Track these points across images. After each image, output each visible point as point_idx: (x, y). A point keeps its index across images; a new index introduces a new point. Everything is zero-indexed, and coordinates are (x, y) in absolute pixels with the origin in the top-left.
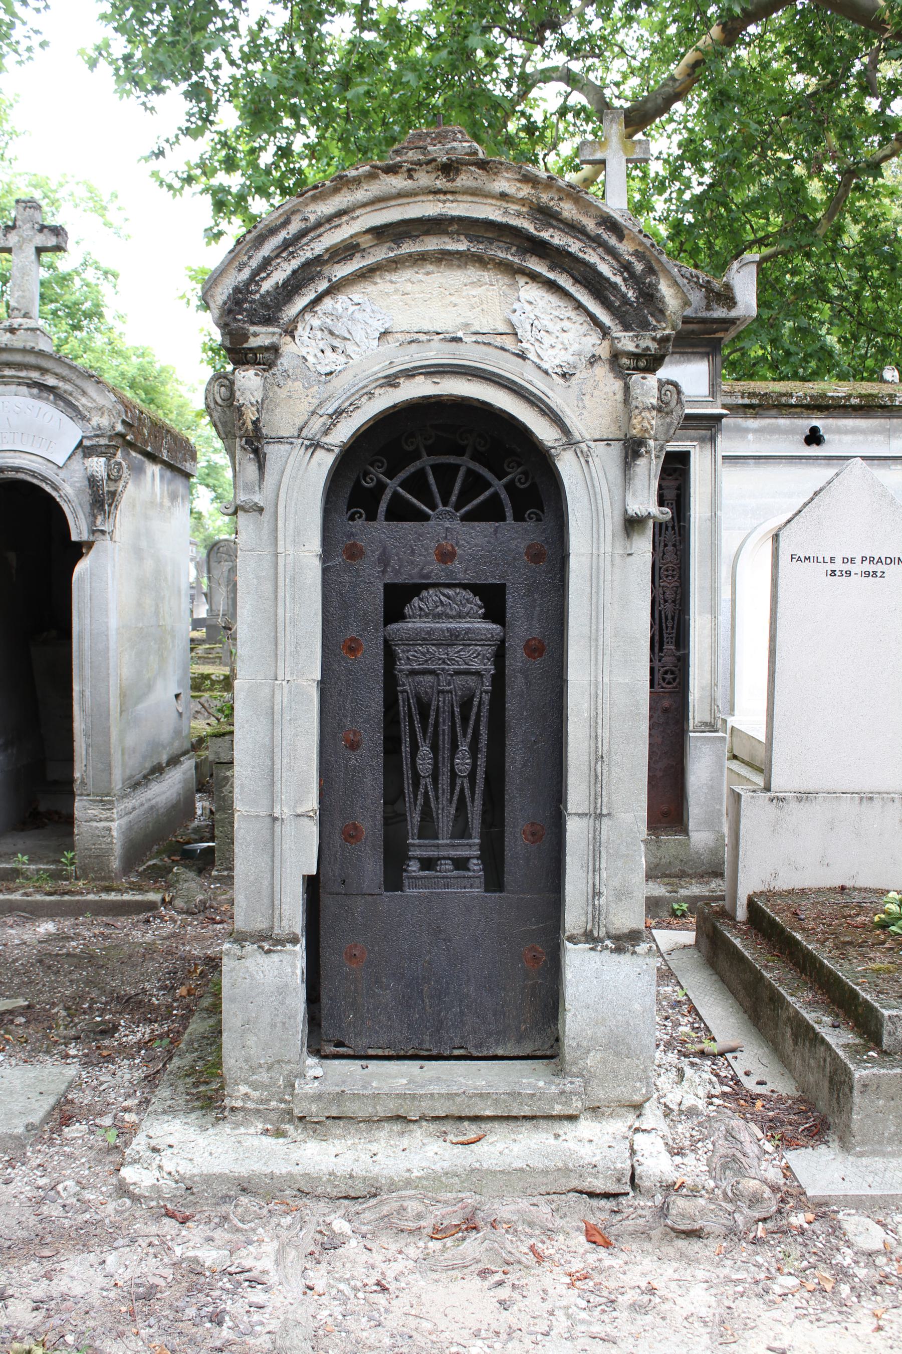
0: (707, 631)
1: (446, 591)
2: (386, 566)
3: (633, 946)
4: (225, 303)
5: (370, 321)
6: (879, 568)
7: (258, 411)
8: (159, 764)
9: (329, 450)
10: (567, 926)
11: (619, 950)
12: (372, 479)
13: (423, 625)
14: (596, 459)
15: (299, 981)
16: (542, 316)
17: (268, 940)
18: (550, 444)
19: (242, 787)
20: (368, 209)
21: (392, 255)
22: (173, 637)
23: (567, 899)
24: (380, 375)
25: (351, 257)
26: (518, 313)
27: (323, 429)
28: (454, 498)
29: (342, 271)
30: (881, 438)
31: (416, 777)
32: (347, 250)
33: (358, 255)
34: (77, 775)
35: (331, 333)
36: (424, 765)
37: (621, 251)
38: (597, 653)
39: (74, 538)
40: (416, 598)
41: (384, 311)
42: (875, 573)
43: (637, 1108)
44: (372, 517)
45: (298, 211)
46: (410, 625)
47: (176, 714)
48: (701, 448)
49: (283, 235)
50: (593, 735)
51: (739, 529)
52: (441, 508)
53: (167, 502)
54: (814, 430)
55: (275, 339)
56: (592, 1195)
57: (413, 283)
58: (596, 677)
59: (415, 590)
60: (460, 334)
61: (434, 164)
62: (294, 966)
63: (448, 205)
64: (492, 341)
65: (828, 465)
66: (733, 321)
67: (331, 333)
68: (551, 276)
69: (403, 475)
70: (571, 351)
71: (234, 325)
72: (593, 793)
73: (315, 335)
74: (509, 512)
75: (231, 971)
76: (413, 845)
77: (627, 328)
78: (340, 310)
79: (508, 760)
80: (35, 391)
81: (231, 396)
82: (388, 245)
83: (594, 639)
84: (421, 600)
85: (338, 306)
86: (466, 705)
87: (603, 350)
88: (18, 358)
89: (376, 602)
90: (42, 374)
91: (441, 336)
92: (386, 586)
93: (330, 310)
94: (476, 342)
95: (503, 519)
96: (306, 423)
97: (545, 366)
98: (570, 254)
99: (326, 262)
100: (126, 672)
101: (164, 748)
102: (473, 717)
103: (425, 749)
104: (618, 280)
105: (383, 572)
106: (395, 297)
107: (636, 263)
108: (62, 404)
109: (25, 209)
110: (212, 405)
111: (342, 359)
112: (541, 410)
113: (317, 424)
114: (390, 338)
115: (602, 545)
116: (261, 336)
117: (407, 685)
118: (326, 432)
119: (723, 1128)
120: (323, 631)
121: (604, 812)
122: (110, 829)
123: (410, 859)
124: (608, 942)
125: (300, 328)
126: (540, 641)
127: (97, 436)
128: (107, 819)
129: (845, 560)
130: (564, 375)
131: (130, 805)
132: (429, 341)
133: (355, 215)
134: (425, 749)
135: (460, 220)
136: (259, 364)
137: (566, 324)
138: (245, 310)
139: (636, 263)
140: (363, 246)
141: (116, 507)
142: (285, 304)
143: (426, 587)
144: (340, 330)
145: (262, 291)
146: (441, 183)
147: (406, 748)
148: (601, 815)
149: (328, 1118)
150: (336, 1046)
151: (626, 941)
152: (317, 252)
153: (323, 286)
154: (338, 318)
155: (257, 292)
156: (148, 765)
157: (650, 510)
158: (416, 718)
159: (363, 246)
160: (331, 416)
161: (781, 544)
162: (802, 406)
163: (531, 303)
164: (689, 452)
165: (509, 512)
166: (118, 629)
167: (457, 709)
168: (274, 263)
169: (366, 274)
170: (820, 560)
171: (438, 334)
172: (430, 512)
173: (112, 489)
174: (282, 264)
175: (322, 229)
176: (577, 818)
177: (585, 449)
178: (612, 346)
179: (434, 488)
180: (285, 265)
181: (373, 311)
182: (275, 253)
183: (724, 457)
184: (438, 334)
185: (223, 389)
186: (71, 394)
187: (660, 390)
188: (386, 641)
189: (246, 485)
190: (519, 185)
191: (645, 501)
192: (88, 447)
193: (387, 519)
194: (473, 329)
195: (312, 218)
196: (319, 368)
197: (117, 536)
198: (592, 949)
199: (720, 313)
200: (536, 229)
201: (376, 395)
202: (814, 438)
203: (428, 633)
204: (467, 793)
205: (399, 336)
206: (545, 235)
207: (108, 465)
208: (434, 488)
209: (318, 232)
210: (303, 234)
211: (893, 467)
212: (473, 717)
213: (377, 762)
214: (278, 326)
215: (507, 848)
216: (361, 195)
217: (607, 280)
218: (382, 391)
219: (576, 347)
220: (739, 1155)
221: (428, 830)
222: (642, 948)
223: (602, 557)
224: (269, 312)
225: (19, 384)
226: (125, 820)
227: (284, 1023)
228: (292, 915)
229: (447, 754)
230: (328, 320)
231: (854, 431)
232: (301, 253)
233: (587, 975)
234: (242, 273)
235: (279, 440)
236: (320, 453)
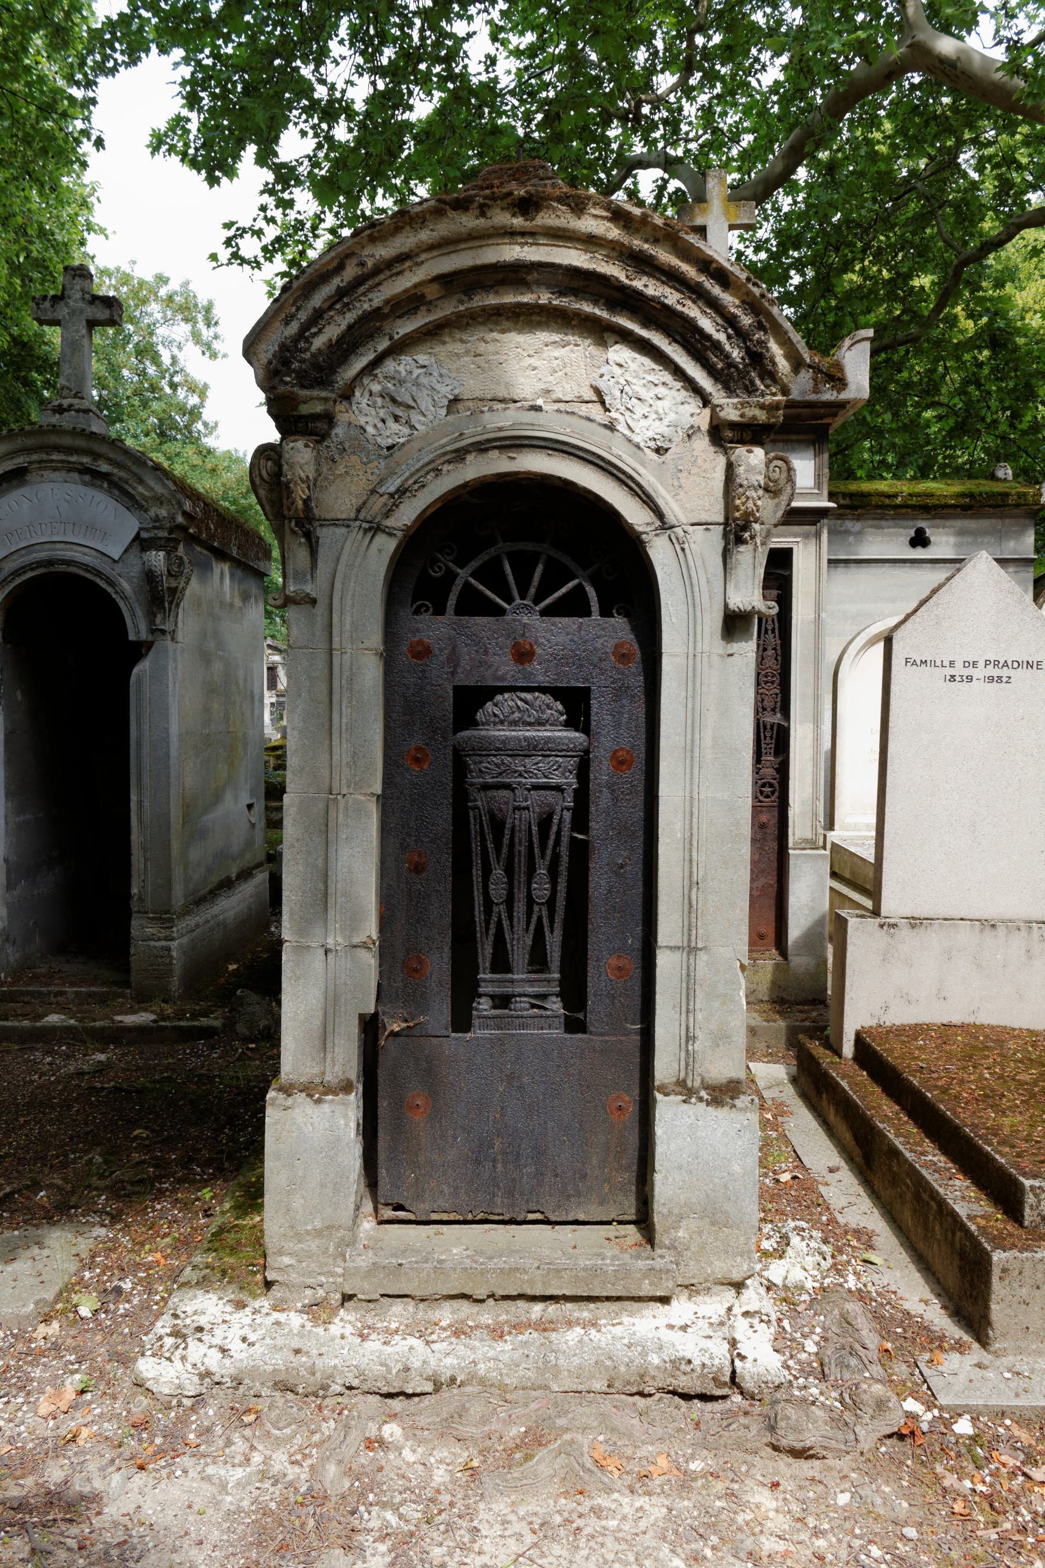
0: (809, 741)
1: (523, 695)
2: (456, 666)
3: (732, 1098)
4: (270, 362)
5: (438, 387)
6: (1005, 672)
7: (308, 488)
8: (228, 878)
9: (390, 535)
10: (657, 1074)
11: (716, 1101)
12: (440, 568)
13: (497, 733)
14: (693, 546)
15: (353, 1135)
16: (634, 381)
18: (640, 529)
20: (435, 253)
21: (462, 308)
22: (246, 744)
23: (657, 1043)
24: (448, 448)
26: (605, 378)
27: (384, 511)
28: (532, 591)
29: (405, 327)
31: (488, 904)
32: (411, 302)
33: (423, 308)
34: (134, 890)
35: (393, 400)
36: (498, 891)
37: (725, 303)
38: (692, 766)
39: (132, 637)
40: (489, 703)
41: (453, 375)
43: (739, 1286)
44: (440, 611)
45: (353, 254)
47: (248, 825)
48: (805, 544)
49: (336, 282)
50: (687, 858)
52: (518, 601)
53: (238, 602)
55: (329, 406)
56: (686, 1397)
57: (486, 342)
58: (691, 792)
59: (489, 693)
60: (540, 402)
61: (509, 200)
62: (346, 1116)
64: (576, 410)
66: (842, 405)
68: (645, 333)
69: (475, 564)
70: (666, 422)
71: (282, 389)
72: (686, 924)
73: (375, 402)
74: (595, 606)
75: (276, 1123)
76: (485, 980)
77: (730, 391)
78: (404, 373)
79: (591, 885)
80: (87, 478)
81: (278, 473)
82: (457, 296)
83: (690, 750)
84: (496, 705)
85: (401, 368)
86: (545, 823)
87: (703, 420)
88: (67, 441)
90: (95, 460)
91: (519, 404)
92: (457, 689)
94: (558, 411)
95: (588, 613)
96: (364, 503)
97: (637, 439)
98: (665, 306)
99: (385, 317)
100: (189, 781)
101: (234, 860)
102: (552, 837)
103: (498, 872)
104: (721, 337)
105: (453, 673)
107: (743, 317)
108: (117, 493)
109: (74, 278)
110: (258, 481)
111: (406, 431)
113: (378, 504)
114: (460, 406)
115: (699, 644)
117: (480, 800)
118: (387, 515)
119: (836, 1312)
120: (385, 739)
121: (699, 946)
122: (169, 949)
123: (480, 996)
124: (703, 1094)
125: (357, 394)
126: (628, 752)
127: (155, 528)
128: (166, 939)
129: (966, 664)
130: (658, 451)
131: (193, 923)
132: (505, 409)
133: (419, 260)
134: (498, 872)
136: (311, 434)
137: (661, 391)
138: (294, 371)
139: (743, 317)
140: (429, 297)
141: (178, 605)
142: (339, 365)
143: (502, 690)
145: (313, 348)
146: (518, 222)
147: (477, 873)
148: (696, 949)
149: (382, 1296)
150: (395, 1209)
151: (723, 1094)
152: (377, 302)
153: (383, 345)
154: (401, 382)
155: (307, 350)
156: (215, 879)
157: (755, 604)
158: (489, 838)
159: (429, 297)
160: (392, 495)
162: (907, 506)
163: (621, 366)
165: (595, 606)
166: (180, 735)
167: (535, 829)
168: (326, 316)
169: (432, 333)
170: (939, 663)
171: (515, 402)
173: (174, 585)
175: (382, 277)
176: (668, 952)
177: (681, 533)
178: (713, 416)
179: (511, 578)
180: (338, 319)
181: (441, 375)
182: (328, 304)
183: (830, 561)
185: (270, 463)
186: (126, 482)
187: (767, 466)
188: (456, 751)
189: (296, 573)
190: (609, 224)
191: (748, 594)
192: (145, 540)
194: (554, 396)
196: (379, 440)
197: (180, 636)
198: (684, 1101)
199: (829, 395)
202: (920, 540)
203: (503, 742)
205: (470, 404)
206: (638, 284)
207: (168, 557)
208: (511, 578)
209: (377, 280)
210: (358, 282)
212: (552, 837)
213: (446, 887)
214: (332, 391)
215: (589, 984)
216: (425, 236)
218: (450, 467)
219: (672, 416)
220: (857, 1346)
221: (501, 964)
222: (743, 1101)
223: (698, 658)
224: (322, 371)
225: (70, 470)
226: (185, 940)
227: (335, 1184)
228: (345, 1059)
229: (523, 878)
230: (389, 385)
232: (358, 305)
233: (680, 1129)
234: (289, 328)
235: (335, 522)
236: (381, 539)
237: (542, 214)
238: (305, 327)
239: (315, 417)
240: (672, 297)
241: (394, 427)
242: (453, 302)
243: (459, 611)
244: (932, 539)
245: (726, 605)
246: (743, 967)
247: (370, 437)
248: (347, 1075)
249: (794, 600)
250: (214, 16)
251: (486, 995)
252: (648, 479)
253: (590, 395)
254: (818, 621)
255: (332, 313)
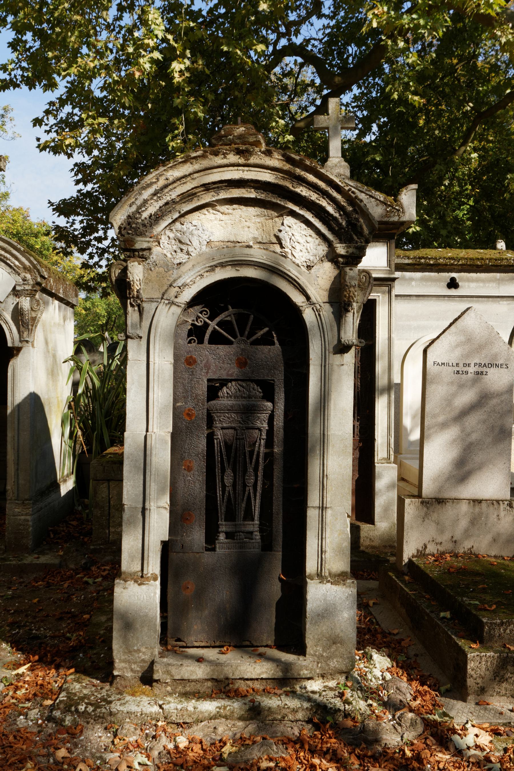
2: (208, 369)
5: (201, 235)
6: (485, 369)
9: (178, 306)
17: (141, 578)
19: (128, 491)
25: (191, 200)
28: (246, 333)
30: (494, 285)
31: (224, 486)
35: (180, 242)
42: (482, 372)
46: (222, 402)
51: (406, 339)
54: (453, 280)
60: (251, 243)
62: (155, 593)
63: (245, 172)
65: (461, 301)
67: (180, 242)
68: (302, 212)
76: (222, 525)
77: (341, 242)
78: (185, 229)
89: (202, 389)
91: (240, 244)
93: (180, 229)
97: (297, 262)
104: (337, 215)
105: (207, 373)
106: (215, 222)
112: (294, 285)
116: (141, 243)
127: (24, 284)
129: (465, 365)
132: (235, 247)
135: (252, 181)
137: (309, 239)
138: (133, 228)
142: (155, 225)
144: (185, 240)
145: (143, 218)
146: (242, 161)
150: (176, 641)
152: (173, 197)
153: (176, 215)
161: (428, 356)
163: (290, 227)
164: (375, 300)
168: (149, 202)
170: (451, 364)
171: (239, 242)
172: (233, 340)
174: (154, 203)
177: (319, 307)
180: (155, 204)
183: (397, 296)
184: (239, 242)
192: (19, 291)
193: (209, 343)
195: (171, 179)
198: (320, 582)
200: (293, 186)
201: (205, 276)
204: (252, 495)
210: (166, 186)
211: (501, 303)
217: (332, 215)
218: (208, 274)
231: (477, 280)
232: (164, 197)
236: (174, 308)
237: (252, 158)
238: (139, 208)
239: (143, 250)
240: (314, 196)
241: (180, 254)
242: (210, 196)
243: (212, 341)
244: (460, 284)
245: (339, 340)
246: (348, 516)
247: (169, 259)
248: (154, 571)
249: (377, 327)
250: (404, 564)
251: (222, 532)
252: (303, 281)
253: (274, 240)
254: (390, 338)
255: (152, 201)
